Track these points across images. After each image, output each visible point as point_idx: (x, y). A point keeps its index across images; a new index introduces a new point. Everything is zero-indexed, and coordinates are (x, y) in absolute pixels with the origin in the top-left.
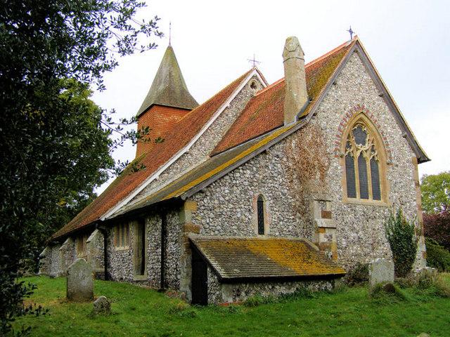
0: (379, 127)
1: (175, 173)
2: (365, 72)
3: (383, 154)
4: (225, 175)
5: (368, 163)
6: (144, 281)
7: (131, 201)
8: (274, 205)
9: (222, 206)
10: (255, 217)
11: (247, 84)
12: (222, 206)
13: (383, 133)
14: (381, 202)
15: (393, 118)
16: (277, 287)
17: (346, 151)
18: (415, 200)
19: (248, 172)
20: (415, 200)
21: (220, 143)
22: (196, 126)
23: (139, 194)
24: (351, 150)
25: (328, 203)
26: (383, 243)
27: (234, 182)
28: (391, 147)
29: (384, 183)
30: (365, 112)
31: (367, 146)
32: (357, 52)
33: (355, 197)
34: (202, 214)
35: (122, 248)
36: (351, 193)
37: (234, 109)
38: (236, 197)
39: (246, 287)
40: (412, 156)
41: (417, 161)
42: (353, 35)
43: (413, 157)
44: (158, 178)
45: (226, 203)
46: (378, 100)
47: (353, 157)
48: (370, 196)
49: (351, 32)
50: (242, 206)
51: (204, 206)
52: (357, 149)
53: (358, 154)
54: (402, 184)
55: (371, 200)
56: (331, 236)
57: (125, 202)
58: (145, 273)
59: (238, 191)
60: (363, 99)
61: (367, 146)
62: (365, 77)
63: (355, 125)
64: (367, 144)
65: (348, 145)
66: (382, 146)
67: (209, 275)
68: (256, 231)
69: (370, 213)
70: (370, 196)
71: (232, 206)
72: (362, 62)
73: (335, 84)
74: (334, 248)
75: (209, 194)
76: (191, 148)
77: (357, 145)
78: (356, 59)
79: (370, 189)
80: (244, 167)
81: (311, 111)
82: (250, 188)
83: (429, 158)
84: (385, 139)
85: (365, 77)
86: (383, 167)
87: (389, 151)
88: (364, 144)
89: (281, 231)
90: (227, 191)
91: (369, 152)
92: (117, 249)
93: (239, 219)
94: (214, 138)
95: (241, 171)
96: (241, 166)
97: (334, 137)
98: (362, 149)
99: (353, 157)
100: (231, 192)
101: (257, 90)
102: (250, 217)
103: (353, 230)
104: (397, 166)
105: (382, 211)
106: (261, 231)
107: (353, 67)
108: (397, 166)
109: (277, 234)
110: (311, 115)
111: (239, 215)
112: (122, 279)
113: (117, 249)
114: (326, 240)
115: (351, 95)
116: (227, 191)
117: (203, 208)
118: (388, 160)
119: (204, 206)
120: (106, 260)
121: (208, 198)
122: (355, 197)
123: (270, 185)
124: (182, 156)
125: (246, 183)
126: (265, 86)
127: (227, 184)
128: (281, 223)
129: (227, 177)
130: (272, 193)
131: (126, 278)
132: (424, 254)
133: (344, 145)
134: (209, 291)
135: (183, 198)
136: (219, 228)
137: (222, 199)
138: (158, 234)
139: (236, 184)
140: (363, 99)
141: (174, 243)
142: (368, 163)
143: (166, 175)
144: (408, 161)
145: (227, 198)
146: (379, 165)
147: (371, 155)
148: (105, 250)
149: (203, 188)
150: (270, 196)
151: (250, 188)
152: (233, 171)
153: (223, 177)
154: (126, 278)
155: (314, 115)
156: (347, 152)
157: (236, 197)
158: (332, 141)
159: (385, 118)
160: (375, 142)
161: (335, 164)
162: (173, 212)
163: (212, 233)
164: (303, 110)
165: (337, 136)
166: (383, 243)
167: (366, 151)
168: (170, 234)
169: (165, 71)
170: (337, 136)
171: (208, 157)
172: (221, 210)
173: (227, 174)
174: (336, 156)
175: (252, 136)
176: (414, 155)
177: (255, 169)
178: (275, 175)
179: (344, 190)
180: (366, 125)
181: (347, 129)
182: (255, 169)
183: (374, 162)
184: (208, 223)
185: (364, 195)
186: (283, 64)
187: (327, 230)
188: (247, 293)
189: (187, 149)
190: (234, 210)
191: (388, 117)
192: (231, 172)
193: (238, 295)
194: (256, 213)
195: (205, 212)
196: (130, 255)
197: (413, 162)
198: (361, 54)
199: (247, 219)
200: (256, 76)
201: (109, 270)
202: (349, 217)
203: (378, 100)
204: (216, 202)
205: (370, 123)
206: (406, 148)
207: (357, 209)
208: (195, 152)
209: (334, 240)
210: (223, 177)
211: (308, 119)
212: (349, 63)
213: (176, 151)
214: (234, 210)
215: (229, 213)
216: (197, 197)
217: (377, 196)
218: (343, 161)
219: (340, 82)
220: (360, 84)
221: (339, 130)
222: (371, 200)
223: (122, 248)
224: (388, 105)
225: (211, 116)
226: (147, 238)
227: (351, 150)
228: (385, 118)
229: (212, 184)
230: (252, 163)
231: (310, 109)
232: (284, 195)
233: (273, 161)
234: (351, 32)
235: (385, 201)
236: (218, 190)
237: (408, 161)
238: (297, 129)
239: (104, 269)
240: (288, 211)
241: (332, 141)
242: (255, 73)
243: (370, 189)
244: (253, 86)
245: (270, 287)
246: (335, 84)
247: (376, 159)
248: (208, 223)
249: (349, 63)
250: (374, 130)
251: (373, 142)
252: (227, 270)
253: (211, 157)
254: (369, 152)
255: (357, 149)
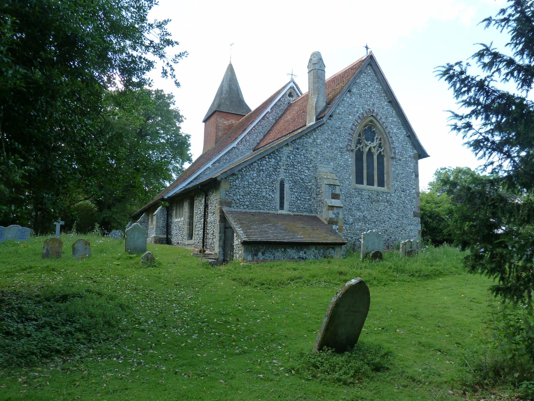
0: (387, 127)
1: (224, 163)
2: (377, 82)
3: (388, 149)
4: (254, 162)
5: (375, 157)
6: (192, 244)
7: (189, 184)
8: (293, 187)
9: (250, 186)
10: (277, 196)
11: (285, 94)
12: (250, 186)
13: (389, 133)
14: (385, 189)
15: (399, 121)
16: (289, 250)
17: (357, 146)
18: (414, 189)
19: (273, 160)
20: (414, 189)
21: (261, 140)
22: (242, 127)
23: (195, 179)
24: (361, 146)
25: (337, 187)
26: (384, 222)
27: (261, 168)
28: (396, 144)
29: (388, 173)
30: (374, 115)
31: (375, 143)
32: (371, 65)
33: (363, 184)
34: (234, 192)
35: (179, 220)
36: (359, 180)
37: (274, 113)
38: (262, 179)
39: (263, 249)
40: (412, 152)
41: (418, 156)
42: (369, 50)
43: (415, 154)
44: (210, 166)
45: (254, 184)
46: (386, 105)
47: (362, 151)
48: (376, 183)
49: (367, 48)
50: (267, 187)
51: (236, 186)
52: (366, 146)
53: (367, 149)
54: (404, 175)
55: (375, 187)
56: (338, 213)
57: (184, 184)
58: (193, 238)
59: (264, 175)
60: (374, 104)
61: (375, 143)
62: (377, 86)
63: (366, 126)
64: (375, 142)
65: (359, 142)
66: (388, 144)
67: (235, 238)
68: (278, 207)
69: (374, 197)
70: (376, 183)
71: (259, 186)
72: (375, 73)
73: (350, 91)
74: (340, 223)
75: (240, 177)
76: (238, 143)
77: (366, 142)
78: (369, 71)
79: (376, 178)
80: (270, 157)
81: (328, 113)
82: (274, 173)
83: (429, 154)
84: (391, 137)
85: (377, 86)
86: (388, 161)
87: (394, 148)
88: (373, 141)
89: (298, 208)
90: (255, 175)
91: (376, 149)
92: (176, 220)
93: (264, 197)
94: (257, 137)
95: (267, 159)
96: (267, 155)
97: (347, 135)
98: (370, 146)
99: (362, 151)
100: (258, 176)
101: (294, 99)
102: (273, 196)
103: (359, 209)
104: (400, 160)
105: (385, 196)
106: (282, 207)
107: (366, 79)
108: (400, 160)
109: (295, 210)
110: (327, 116)
111: (264, 194)
112: (178, 243)
113: (176, 220)
114: (334, 216)
115: (363, 101)
116: (255, 175)
117: (235, 187)
118: (393, 155)
119: (236, 186)
120: (167, 230)
121: (239, 179)
122: (363, 184)
123: (290, 172)
124: (231, 150)
125: (271, 169)
126: (300, 95)
127: (255, 169)
128: (299, 201)
129: (255, 164)
130: (292, 177)
131: (181, 243)
132: (419, 232)
133: (354, 141)
134: (234, 251)
135: (219, 179)
136: (247, 203)
137: (250, 181)
138: (202, 208)
139: (263, 169)
140: (374, 104)
141: (212, 214)
142: (375, 157)
143: (217, 164)
144: (410, 157)
145: (255, 180)
146: (385, 159)
147: (378, 150)
148: (167, 221)
149: (236, 172)
150: (290, 180)
151: (274, 173)
152: (261, 159)
153: (252, 164)
154: (181, 243)
155: (331, 116)
156: (358, 148)
157: (262, 179)
158: (344, 138)
159: (393, 121)
160: (382, 140)
161: (346, 157)
162: (212, 191)
163: (242, 207)
164: (321, 112)
165: (350, 134)
166: (384, 222)
167: (374, 147)
168: (210, 208)
169: (226, 87)
170: (350, 134)
171: (252, 151)
172: (250, 190)
173: (256, 162)
174: (348, 150)
175: (284, 134)
176: (415, 151)
177: (278, 158)
178: (295, 163)
179: (353, 178)
180: (375, 126)
181: (359, 129)
182: (278, 158)
183: (381, 157)
184: (239, 200)
185: (370, 183)
186: (307, 74)
187: (335, 208)
188: (263, 254)
189: (234, 144)
190: (260, 190)
191: (395, 120)
192: (258, 160)
193: (256, 255)
194: (278, 193)
195: (237, 190)
196: (184, 225)
197: (414, 158)
198: (374, 66)
199: (270, 197)
200: (293, 87)
201: (169, 236)
202: (356, 200)
203: (386, 105)
204: (246, 183)
205: (378, 125)
206: (409, 146)
207: (363, 193)
208: (241, 147)
209: (341, 216)
210: (252, 164)
211: (325, 119)
212: (363, 74)
213: (226, 146)
214: (260, 190)
215: (256, 192)
216: (230, 178)
217: (381, 183)
218: (353, 155)
219: (354, 90)
220: (372, 92)
221: (352, 129)
222: (375, 187)
223: (179, 220)
224: (395, 110)
225: (255, 119)
226: (195, 211)
227: (361, 146)
228: (393, 121)
229: (242, 169)
230: (277, 153)
231: (327, 112)
232: (302, 179)
233: (294, 153)
234: (367, 48)
235: (388, 188)
236: (248, 173)
237: (410, 157)
238: (315, 127)
239: (166, 236)
240: (305, 193)
241: (344, 138)
242: (292, 84)
243: (376, 178)
244: (290, 95)
245: (283, 250)
246: (350, 91)
247: (383, 154)
248: (239, 200)
249: (363, 74)
250: (382, 130)
251: (380, 140)
252: (248, 236)
253: (254, 151)
254: (376, 149)
255: (366, 146)
